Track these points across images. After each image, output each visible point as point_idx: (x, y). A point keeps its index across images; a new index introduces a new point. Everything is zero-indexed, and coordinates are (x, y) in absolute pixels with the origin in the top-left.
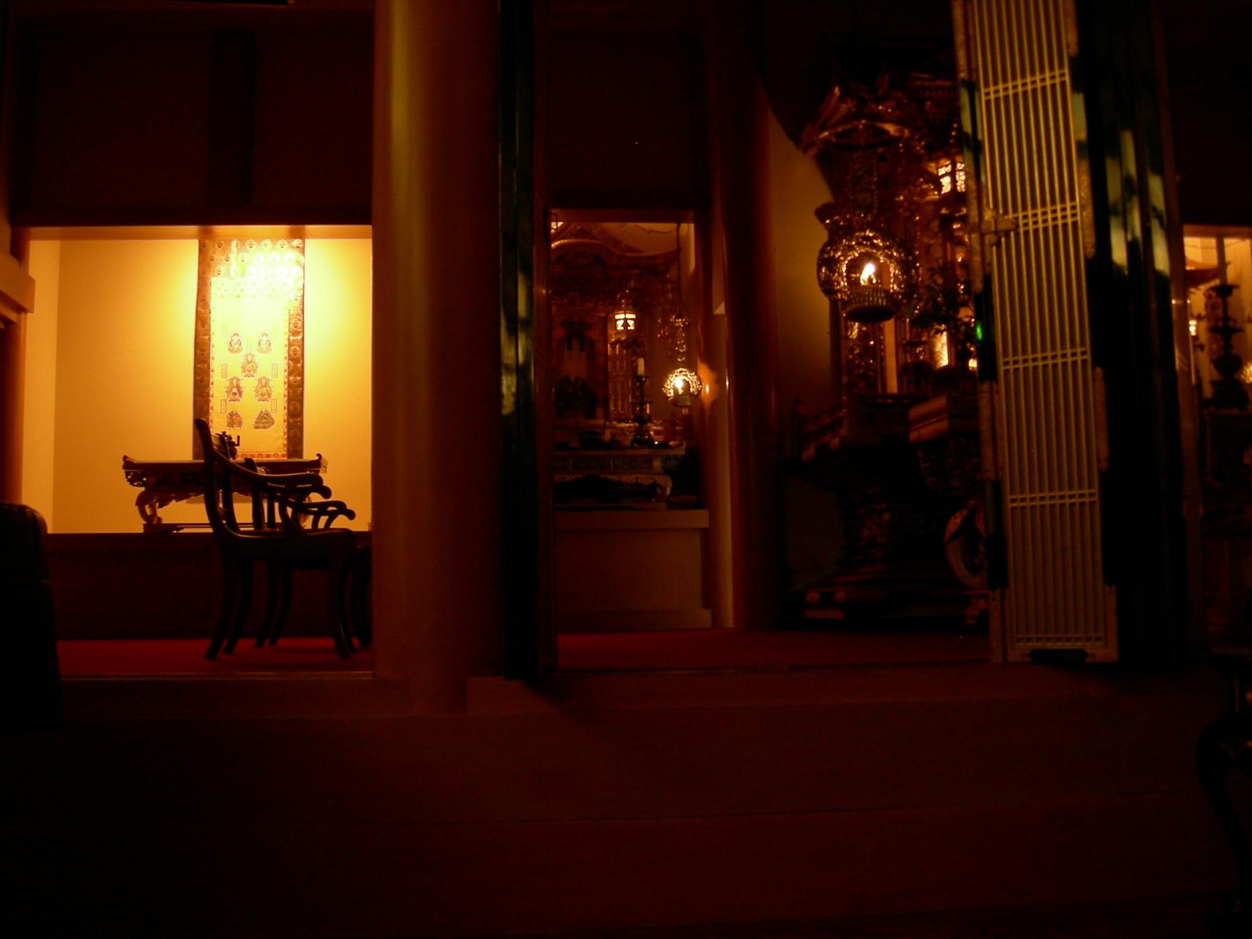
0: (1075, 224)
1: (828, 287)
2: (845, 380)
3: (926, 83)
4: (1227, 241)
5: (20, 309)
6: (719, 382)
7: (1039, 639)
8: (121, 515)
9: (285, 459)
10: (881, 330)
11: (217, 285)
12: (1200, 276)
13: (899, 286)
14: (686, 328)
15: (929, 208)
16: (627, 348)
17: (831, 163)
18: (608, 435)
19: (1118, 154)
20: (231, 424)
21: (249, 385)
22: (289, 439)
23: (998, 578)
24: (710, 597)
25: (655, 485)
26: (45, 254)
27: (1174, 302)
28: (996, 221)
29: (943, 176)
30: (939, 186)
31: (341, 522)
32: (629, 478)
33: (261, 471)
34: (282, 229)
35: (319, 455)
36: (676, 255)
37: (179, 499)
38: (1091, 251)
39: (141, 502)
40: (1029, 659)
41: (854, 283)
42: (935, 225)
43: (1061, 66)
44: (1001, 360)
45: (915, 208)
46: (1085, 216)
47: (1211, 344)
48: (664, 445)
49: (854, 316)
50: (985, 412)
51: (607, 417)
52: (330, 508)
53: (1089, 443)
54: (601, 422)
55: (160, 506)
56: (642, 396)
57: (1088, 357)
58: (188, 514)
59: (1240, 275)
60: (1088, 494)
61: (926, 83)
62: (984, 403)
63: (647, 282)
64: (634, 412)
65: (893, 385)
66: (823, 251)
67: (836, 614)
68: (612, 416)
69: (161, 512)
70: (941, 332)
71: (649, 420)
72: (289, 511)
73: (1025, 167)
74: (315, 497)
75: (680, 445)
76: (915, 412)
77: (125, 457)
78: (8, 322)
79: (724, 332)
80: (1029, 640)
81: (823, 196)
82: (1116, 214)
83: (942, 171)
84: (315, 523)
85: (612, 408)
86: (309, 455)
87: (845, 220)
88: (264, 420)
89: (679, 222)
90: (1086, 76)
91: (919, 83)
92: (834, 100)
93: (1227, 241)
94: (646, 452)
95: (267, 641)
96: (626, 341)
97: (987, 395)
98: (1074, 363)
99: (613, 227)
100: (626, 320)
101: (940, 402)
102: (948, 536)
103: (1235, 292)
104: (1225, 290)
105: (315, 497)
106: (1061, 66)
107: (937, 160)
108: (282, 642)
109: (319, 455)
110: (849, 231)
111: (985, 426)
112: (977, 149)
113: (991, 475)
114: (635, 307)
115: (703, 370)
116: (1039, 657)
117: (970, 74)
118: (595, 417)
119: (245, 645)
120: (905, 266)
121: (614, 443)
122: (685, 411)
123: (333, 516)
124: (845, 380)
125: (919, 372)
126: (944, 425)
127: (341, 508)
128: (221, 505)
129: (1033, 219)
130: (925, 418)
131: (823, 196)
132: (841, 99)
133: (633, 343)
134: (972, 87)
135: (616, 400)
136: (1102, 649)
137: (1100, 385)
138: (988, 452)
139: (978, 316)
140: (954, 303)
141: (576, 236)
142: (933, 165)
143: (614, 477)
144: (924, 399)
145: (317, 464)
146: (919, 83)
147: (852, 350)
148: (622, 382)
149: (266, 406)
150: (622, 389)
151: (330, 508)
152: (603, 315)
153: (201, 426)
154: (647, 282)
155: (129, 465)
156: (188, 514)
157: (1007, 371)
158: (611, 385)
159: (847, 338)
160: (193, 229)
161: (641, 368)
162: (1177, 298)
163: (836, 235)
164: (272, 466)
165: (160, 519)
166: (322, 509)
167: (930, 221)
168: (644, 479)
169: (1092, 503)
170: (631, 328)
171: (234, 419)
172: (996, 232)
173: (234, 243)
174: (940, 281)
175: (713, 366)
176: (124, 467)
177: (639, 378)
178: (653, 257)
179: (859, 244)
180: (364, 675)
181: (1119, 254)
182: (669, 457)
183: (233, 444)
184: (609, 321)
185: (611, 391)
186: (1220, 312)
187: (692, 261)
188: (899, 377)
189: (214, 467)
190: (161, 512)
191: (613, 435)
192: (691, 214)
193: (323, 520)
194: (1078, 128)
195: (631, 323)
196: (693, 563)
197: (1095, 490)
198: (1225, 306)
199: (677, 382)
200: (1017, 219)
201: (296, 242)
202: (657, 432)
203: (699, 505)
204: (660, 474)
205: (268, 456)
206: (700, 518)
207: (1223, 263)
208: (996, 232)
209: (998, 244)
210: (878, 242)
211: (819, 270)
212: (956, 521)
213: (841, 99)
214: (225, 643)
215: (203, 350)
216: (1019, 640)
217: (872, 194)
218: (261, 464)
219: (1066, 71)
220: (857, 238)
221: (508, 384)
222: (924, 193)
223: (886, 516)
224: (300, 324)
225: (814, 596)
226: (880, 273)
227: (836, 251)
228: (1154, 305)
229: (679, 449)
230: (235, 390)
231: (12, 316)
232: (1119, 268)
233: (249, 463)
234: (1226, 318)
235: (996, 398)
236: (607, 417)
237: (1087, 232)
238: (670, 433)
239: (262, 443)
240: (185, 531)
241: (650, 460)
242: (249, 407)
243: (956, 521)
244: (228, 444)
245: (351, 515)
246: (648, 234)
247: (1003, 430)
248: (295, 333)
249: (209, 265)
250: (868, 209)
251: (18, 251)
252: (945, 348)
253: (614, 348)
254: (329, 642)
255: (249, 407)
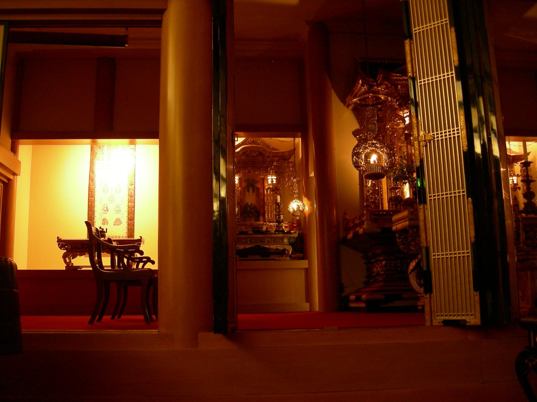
0: (458, 136)
1: (357, 165)
2: (365, 204)
3: (398, 78)
4: (527, 143)
5: (14, 174)
6: (312, 205)
7: (446, 315)
8: (55, 261)
9: (127, 239)
10: (381, 182)
11: (97, 162)
12: (516, 158)
13: (387, 164)
14: (298, 182)
15: (401, 131)
16: (273, 191)
17: (358, 111)
18: (264, 228)
19: (477, 106)
20: (104, 224)
21: (111, 207)
22: (128, 229)
23: (428, 289)
24: (309, 298)
25: (285, 250)
26: (26, 150)
27: (502, 169)
28: (425, 136)
29: (406, 117)
30: (404, 121)
31: (149, 266)
32: (274, 247)
33: (115, 244)
34: (126, 141)
35: (141, 237)
36: (293, 151)
37: (81, 255)
38: (466, 148)
39: (65, 256)
40: (442, 324)
41: (367, 162)
42: (403, 138)
43: (451, 70)
44: (428, 195)
45: (394, 131)
46: (463, 133)
47: (523, 187)
48: (289, 232)
49: (369, 177)
50: (421, 217)
51: (264, 221)
52: (144, 260)
53: (468, 231)
54: (261, 222)
55: (73, 258)
56: (279, 212)
57: (465, 193)
58: (82, 261)
59: (535, 158)
60: (467, 252)
61: (398, 78)
62: (421, 214)
63: (281, 162)
64: (276, 219)
65: (386, 206)
66: (354, 149)
67: (363, 305)
68: (266, 220)
69: (73, 261)
70: (406, 183)
71: (282, 222)
72: (125, 260)
73: (439, 111)
74: (138, 255)
75: (295, 232)
76: (395, 218)
77: (58, 237)
78: (9, 179)
79: (314, 184)
80: (442, 316)
81: (356, 126)
82: (476, 132)
83: (405, 115)
84: (137, 266)
85: (266, 217)
86: (137, 237)
87: (365, 136)
88: (118, 222)
89: (295, 137)
90: (463, 73)
91: (395, 78)
92: (359, 85)
93: (527, 143)
94: (281, 235)
95: (117, 317)
96: (272, 188)
97: (422, 210)
98: (459, 196)
99: (267, 140)
100: (272, 179)
101: (405, 213)
102: (410, 271)
103: (531, 164)
104: (527, 165)
105: (138, 255)
106: (451, 70)
107: (403, 110)
108: (123, 317)
109: (141, 237)
110: (365, 140)
111: (422, 224)
112: (416, 105)
113: (425, 244)
114: (277, 173)
115: (305, 200)
116: (447, 323)
117: (413, 74)
118: (259, 220)
119: (107, 318)
120: (390, 155)
121: (267, 232)
122: (298, 218)
123: (145, 263)
124: (365, 204)
125: (397, 201)
126: (407, 223)
127: (149, 260)
128: (96, 258)
129: (441, 135)
130: (398, 220)
131: (356, 126)
132: (362, 85)
133: (275, 189)
134: (414, 79)
135: (268, 213)
136: (474, 319)
137: (471, 206)
138: (423, 235)
139: (418, 176)
140: (411, 172)
141: (251, 144)
142: (401, 112)
143: (267, 246)
144: (398, 212)
145: (140, 241)
146: (395, 78)
147: (368, 191)
148: (271, 206)
149: (118, 216)
150: (271, 209)
151: (144, 260)
152: (263, 177)
153: (89, 225)
154: (281, 162)
155: (59, 240)
156: (82, 261)
157: (430, 200)
158: (266, 207)
159: (366, 186)
160: (88, 141)
161: (279, 200)
162: (503, 168)
163: (362, 142)
164: (120, 242)
165: (72, 264)
166: (140, 260)
167: (401, 136)
168: (280, 247)
169: (468, 256)
170: (275, 182)
171: (105, 221)
172: (425, 141)
173: (106, 146)
174: (405, 162)
175: (309, 199)
176: (57, 242)
177: (278, 204)
178: (283, 152)
179: (370, 146)
180: (154, 331)
181: (478, 149)
182: (291, 238)
183: (104, 232)
184: (264, 180)
185: (266, 209)
186: (525, 173)
187: (300, 154)
188: (389, 202)
189: (95, 242)
190: (73, 261)
191: (267, 229)
192: (300, 134)
193: (141, 265)
194: (459, 95)
195: (274, 180)
196: (299, 284)
197: (469, 251)
198: (527, 172)
199: (294, 205)
200: (434, 135)
201: (133, 146)
202: (286, 227)
203: (303, 258)
204: (287, 245)
205: (119, 237)
206: (304, 264)
207: (526, 154)
208: (425, 141)
209: (426, 146)
210: (378, 145)
211: (353, 157)
212: (413, 264)
213: (362, 85)
214: (97, 317)
215: (92, 192)
216: (438, 316)
217: (375, 124)
218: (114, 241)
219: (454, 72)
220: (369, 143)
221: (216, 206)
222: (398, 124)
223: (384, 263)
224: (133, 181)
225: (353, 297)
226: (379, 158)
227: (359, 149)
228: (493, 171)
229: (295, 234)
230: (105, 209)
231: (11, 177)
232: (478, 155)
233: (110, 240)
234: (527, 176)
235: (426, 211)
236: (264, 221)
237: (464, 140)
238: (292, 227)
239: (116, 232)
240: (83, 269)
241: (282, 239)
242: (111, 217)
243: (413, 264)
244: (102, 233)
245: (153, 263)
246: (282, 143)
247: (429, 225)
248: (131, 185)
249: (95, 156)
250: (373, 131)
251: (14, 150)
252: (408, 190)
253: (267, 191)
254: (142, 317)
255: (111, 217)
